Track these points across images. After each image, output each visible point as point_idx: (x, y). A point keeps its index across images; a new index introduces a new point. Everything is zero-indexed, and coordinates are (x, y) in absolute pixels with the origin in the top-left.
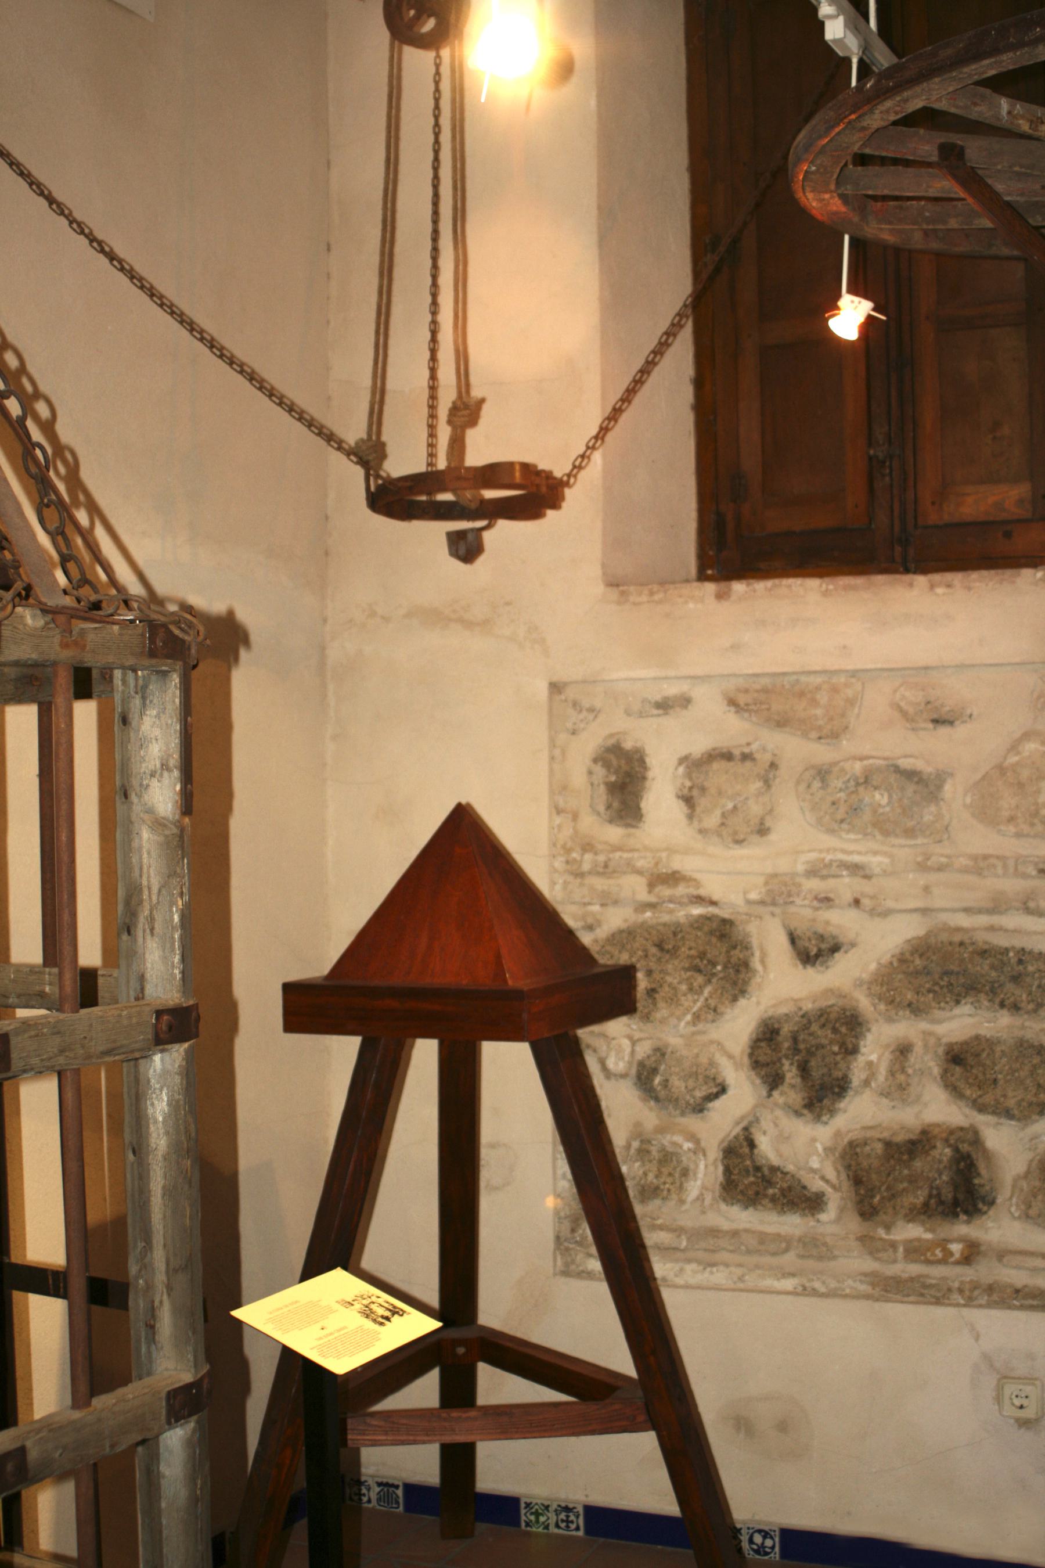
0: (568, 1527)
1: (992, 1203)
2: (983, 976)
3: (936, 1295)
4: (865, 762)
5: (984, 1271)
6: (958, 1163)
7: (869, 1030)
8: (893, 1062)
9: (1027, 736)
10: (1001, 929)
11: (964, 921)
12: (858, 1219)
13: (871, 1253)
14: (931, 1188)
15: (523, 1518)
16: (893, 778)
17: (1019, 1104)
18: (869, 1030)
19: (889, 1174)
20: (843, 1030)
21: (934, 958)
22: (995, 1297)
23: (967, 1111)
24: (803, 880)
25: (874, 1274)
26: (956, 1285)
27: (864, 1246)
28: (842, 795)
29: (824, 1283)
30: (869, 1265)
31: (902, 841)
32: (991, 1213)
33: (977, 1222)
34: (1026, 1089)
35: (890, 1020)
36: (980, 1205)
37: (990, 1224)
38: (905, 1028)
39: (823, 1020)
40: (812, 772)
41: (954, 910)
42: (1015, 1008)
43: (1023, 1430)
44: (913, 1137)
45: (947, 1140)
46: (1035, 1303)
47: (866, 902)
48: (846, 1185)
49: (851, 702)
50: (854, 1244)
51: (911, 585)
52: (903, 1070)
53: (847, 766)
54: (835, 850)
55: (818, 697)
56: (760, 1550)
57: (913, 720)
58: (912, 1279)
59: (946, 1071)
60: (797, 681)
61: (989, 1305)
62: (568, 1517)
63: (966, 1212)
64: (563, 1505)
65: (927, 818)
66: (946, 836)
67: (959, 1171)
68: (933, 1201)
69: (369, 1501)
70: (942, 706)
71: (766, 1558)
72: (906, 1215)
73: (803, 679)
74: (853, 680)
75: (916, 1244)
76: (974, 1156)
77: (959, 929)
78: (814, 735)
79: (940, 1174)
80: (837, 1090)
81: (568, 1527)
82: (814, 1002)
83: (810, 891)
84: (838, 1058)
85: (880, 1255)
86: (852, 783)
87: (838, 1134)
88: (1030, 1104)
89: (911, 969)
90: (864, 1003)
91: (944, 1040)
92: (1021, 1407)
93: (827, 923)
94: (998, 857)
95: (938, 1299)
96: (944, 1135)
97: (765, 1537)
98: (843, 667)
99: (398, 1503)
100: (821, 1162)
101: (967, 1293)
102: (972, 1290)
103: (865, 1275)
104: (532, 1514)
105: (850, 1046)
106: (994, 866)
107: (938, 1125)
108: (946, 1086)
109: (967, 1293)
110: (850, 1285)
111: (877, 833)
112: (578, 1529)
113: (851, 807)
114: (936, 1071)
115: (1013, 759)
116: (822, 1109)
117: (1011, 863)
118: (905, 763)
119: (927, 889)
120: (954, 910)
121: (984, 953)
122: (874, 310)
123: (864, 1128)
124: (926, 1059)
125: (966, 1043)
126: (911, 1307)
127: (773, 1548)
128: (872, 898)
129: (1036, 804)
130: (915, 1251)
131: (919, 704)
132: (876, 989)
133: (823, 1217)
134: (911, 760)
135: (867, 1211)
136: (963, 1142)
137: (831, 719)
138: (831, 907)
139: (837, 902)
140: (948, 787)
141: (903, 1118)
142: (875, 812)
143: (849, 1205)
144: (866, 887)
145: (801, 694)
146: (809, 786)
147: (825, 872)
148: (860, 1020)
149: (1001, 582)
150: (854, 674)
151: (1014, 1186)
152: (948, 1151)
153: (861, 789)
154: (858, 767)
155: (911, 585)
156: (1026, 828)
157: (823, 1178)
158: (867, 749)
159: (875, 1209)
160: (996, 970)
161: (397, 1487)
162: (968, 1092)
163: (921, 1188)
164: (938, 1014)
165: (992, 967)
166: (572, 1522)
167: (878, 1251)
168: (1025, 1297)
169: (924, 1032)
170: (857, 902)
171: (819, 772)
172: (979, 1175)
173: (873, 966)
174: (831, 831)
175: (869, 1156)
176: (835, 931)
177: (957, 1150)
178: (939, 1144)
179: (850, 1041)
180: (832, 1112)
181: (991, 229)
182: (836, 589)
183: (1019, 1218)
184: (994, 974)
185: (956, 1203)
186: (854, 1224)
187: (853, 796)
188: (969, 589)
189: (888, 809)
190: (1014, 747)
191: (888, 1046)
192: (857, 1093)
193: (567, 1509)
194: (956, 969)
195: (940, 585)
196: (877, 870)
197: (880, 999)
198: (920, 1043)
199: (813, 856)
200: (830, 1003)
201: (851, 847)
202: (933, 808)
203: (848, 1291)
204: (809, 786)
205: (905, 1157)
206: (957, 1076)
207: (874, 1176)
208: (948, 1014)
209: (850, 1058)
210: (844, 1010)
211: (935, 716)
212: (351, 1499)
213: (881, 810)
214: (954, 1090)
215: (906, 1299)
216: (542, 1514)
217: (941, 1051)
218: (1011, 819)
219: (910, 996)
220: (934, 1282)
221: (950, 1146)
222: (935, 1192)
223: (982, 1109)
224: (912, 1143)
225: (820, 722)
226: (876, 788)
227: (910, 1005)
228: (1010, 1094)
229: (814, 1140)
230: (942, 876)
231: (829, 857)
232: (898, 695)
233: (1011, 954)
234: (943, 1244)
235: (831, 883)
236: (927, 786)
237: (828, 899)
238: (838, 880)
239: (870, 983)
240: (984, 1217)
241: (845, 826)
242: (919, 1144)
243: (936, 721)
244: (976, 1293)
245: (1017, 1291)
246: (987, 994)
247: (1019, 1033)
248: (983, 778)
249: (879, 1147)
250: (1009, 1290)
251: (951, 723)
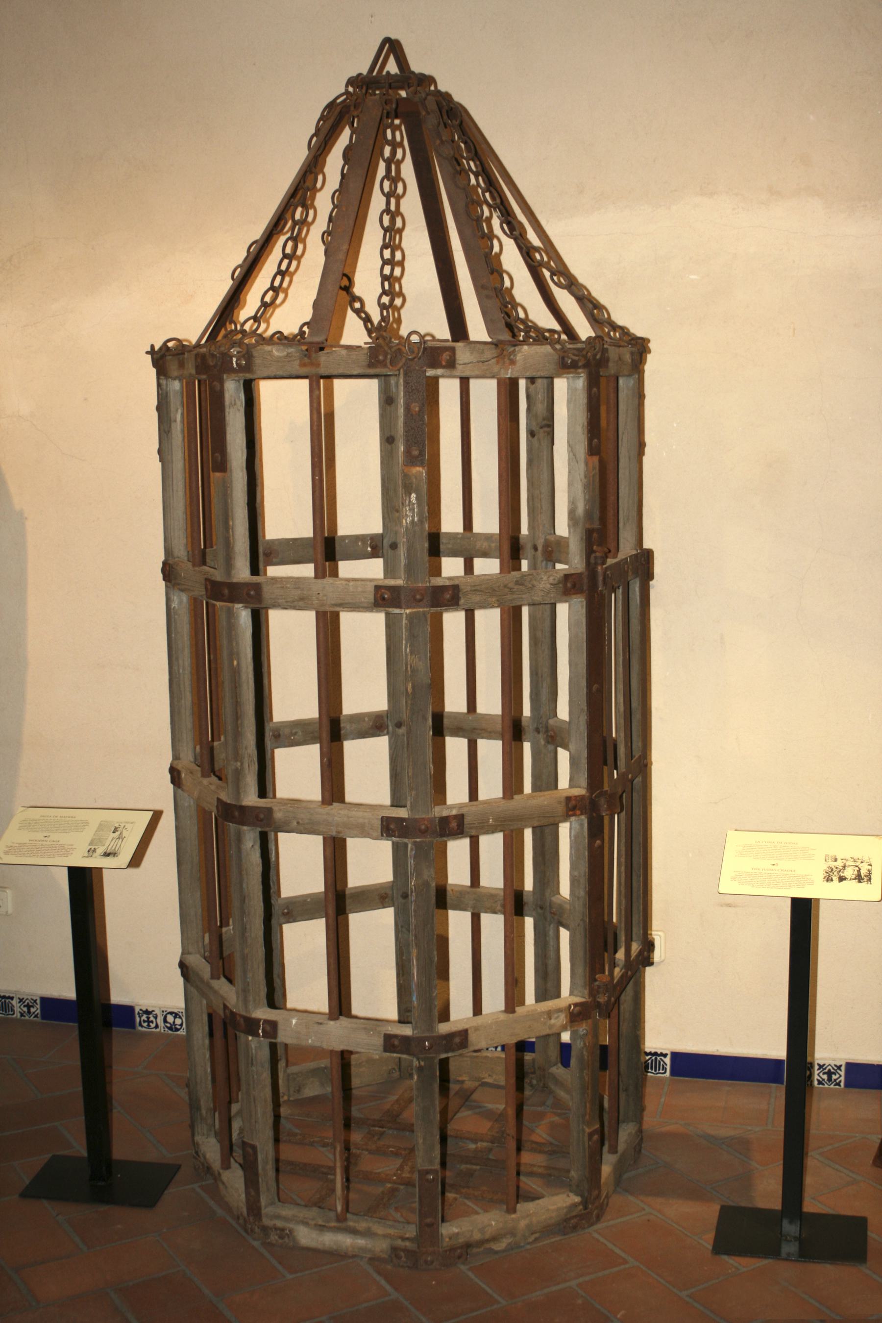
0: (149, 1025)
15: (816, 1077)
56: (173, 1028)
62: (148, 1018)
69: (157, 1026)
71: (178, 1033)
81: (149, 1025)
97: (175, 1017)
99: (665, 1069)
104: (824, 1073)
127: (181, 1025)
161: (665, 1055)
166: (152, 1022)
212: (140, 1025)
216: (33, 1007)
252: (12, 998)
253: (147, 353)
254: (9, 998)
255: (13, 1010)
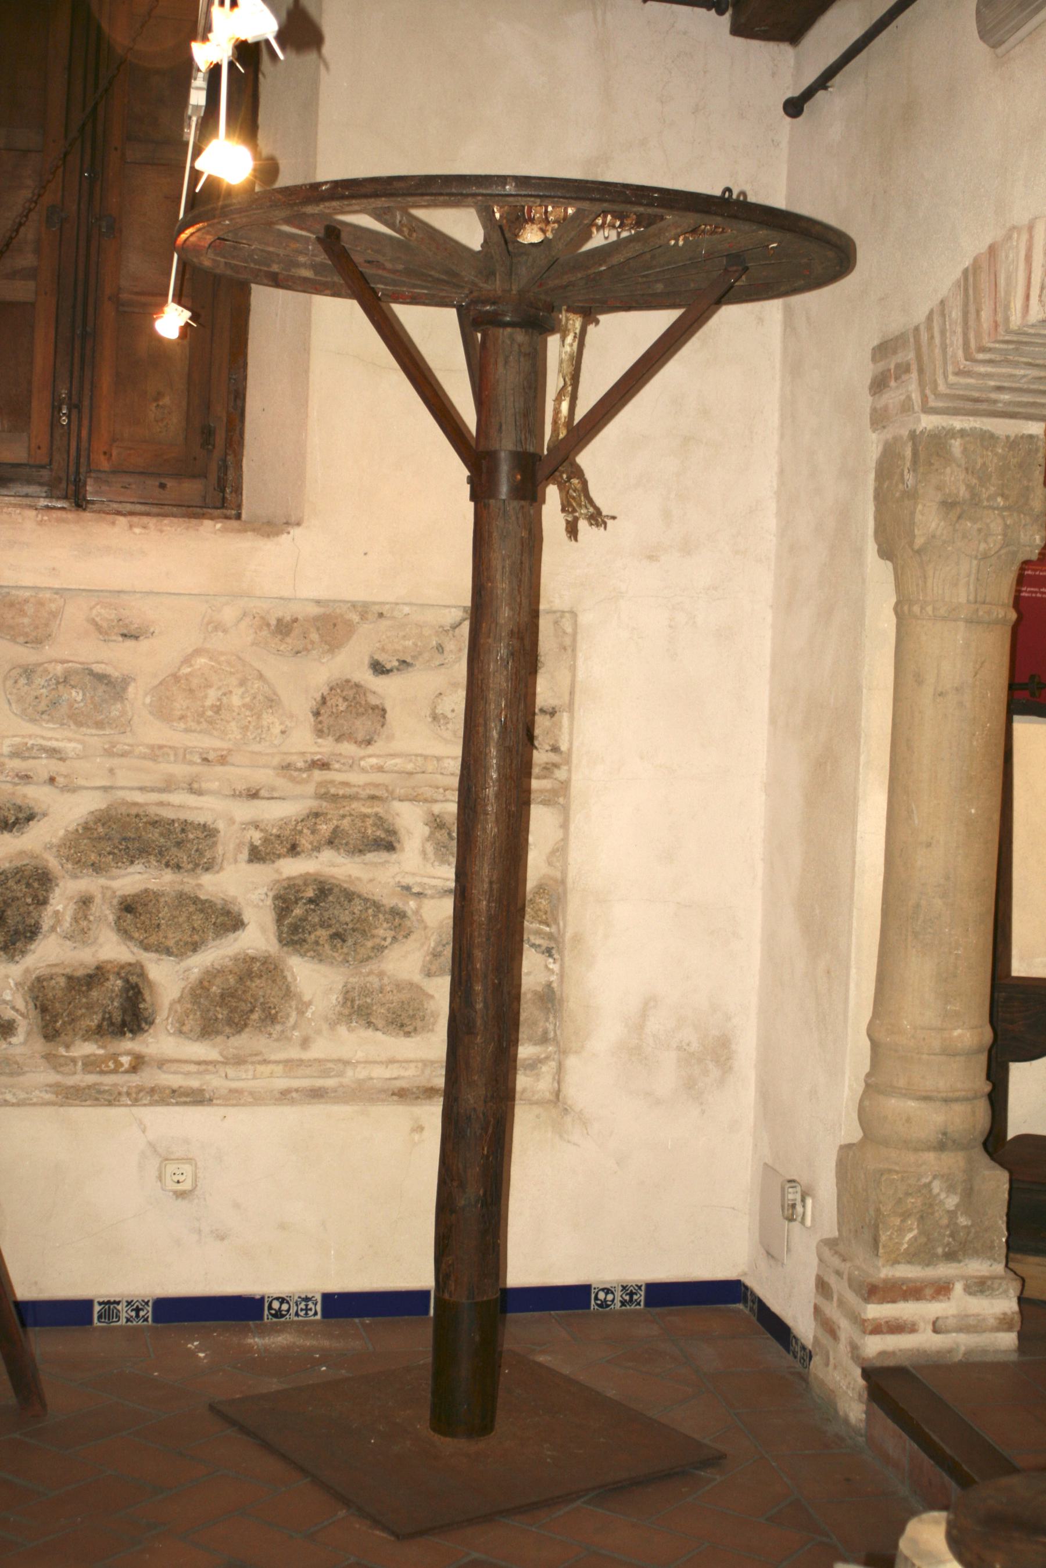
0: (306, 1314)
1: (151, 1023)
2: (153, 841)
3: (109, 1098)
4: (65, 665)
5: (147, 1078)
6: (127, 991)
7: (57, 885)
8: (76, 912)
9: (197, 652)
10: (169, 804)
11: (139, 797)
12: (43, 1040)
13: (54, 1068)
14: (105, 1012)
16: (88, 678)
17: (177, 943)
18: (57, 885)
19: (70, 1003)
20: (36, 885)
21: (114, 826)
22: (156, 1097)
23: (135, 950)
24: (7, 760)
25: (58, 1085)
26: (125, 1089)
27: (49, 1062)
28: (44, 691)
29: (14, 1094)
30: (53, 1077)
31: (94, 731)
32: (151, 1031)
33: (140, 1038)
34: (183, 931)
35: (75, 877)
36: (143, 1025)
37: (150, 1040)
38: (88, 883)
39: (18, 876)
40: (19, 670)
41: (131, 789)
42: (178, 867)
43: (180, 1200)
44: (90, 972)
45: (118, 974)
46: (188, 1100)
47: (60, 780)
48: (33, 1013)
49: (54, 615)
50: (41, 1061)
51: (113, 523)
52: (86, 918)
53: (50, 667)
54: (37, 736)
55: (26, 608)
57: (106, 633)
58: (89, 1087)
59: (119, 918)
60: (8, 593)
61: (151, 1104)
62: (307, 1305)
63: (131, 1031)
64: (303, 1296)
65: (115, 713)
66: (129, 729)
67: (128, 998)
68: (105, 1023)
70: (131, 623)
72: (83, 1036)
73: (14, 592)
74: (57, 597)
75: (92, 1058)
76: (141, 986)
77: (135, 804)
78: (21, 639)
79: (112, 1000)
80: (28, 935)
81: (306, 1314)
82: (11, 862)
83: (12, 769)
84: (31, 908)
85: (62, 1069)
86: (54, 681)
87: (27, 971)
88: (186, 943)
89: (95, 835)
90: (53, 863)
91: (119, 893)
92: (178, 1182)
93: (25, 796)
94: (170, 747)
95: (110, 1101)
96: (116, 969)
98: (51, 585)
100: (13, 995)
101: (134, 1095)
102: (138, 1093)
103: (50, 1086)
105: (41, 898)
106: (168, 755)
107: (111, 962)
108: (119, 930)
109: (134, 1095)
110: (37, 1095)
111: (71, 723)
112: (316, 1314)
113: (51, 701)
114: (111, 918)
115: (186, 670)
116: (15, 950)
117: (181, 752)
118: (98, 668)
119: (111, 771)
120: (131, 789)
121: (155, 823)
122: (191, 319)
123: (49, 966)
124: (103, 907)
125: (136, 895)
126: (90, 1109)
128: (66, 776)
129: (203, 707)
130: (91, 1064)
131: (112, 621)
132: (64, 851)
133: (14, 1040)
134: (103, 666)
135: (51, 1034)
136: (132, 974)
137: (37, 628)
138: (29, 783)
139: (35, 779)
140: (131, 689)
141: (84, 957)
142: (71, 707)
143: (35, 1029)
144: (61, 768)
145: (12, 605)
146: (16, 682)
147: (27, 755)
148: (50, 876)
149: (187, 528)
150: (57, 592)
151: (170, 1009)
152: (119, 982)
153: (61, 687)
154: (59, 669)
155: (113, 523)
156: (193, 725)
157: (13, 1008)
158: (65, 654)
159: (57, 1031)
160: (164, 837)
162: (136, 935)
163: (96, 1013)
164: (115, 872)
165: (161, 834)
166: (311, 1309)
167: (61, 1065)
168: (180, 1096)
169: (102, 887)
170: (52, 780)
171: (25, 671)
172: (144, 1000)
173: (61, 833)
174: (33, 721)
175: (53, 988)
176: (32, 804)
177: (127, 981)
178: (111, 977)
179: (41, 894)
180: (23, 953)
181: (176, 239)
182: (50, 520)
183: (174, 1034)
184: (162, 840)
185: (124, 1024)
186: (39, 1045)
187: (53, 693)
188: (161, 531)
189: (82, 704)
190: (187, 660)
191: (72, 898)
192: (45, 936)
193: (307, 1299)
194: (133, 836)
195: (137, 526)
196: (72, 754)
197: (67, 860)
198: (100, 896)
199: (18, 740)
200: (25, 863)
201: (50, 734)
202: (119, 706)
203: (35, 1100)
204: (16, 682)
205: (84, 988)
206: (128, 922)
207: (57, 1005)
208: (123, 872)
209: (41, 908)
210: (37, 868)
211: (125, 631)
213: (76, 705)
214: (124, 933)
215: (84, 1103)
217: (115, 902)
218: (182, 718)
219: (93, 857)
220: (107, 1088)
221: (121, 978)
222: (107, 1016)
223: (147, 948)
224: (90, 976)
225: (27, 630)
226: (73, 687)
227: (93, 865)
228: (170, 935)
229: (7, 977)
230: (124, 761)
231: (30, 742)
232: (94, 612)
233: (176, 825)
234: (115, 1057)
235: (31, 763)
236: (114, 687)
237: (27, 777)
238: (37, 761)
239: (60, 846)
240: (146, 1035)
241: (45, 717)
242: (96, 976)
243: (124, 635)
244: (141, 1094)
245: (174, 1091)
246: (156, 856)
247: (180, 888)
248: (161, 683)
249: (63, 982)
250: (167, 1091)
251: (137, 638)
252: (118, 1303)
253: (597, 518)
254: (115, 1302)
255: (118, 1317)
